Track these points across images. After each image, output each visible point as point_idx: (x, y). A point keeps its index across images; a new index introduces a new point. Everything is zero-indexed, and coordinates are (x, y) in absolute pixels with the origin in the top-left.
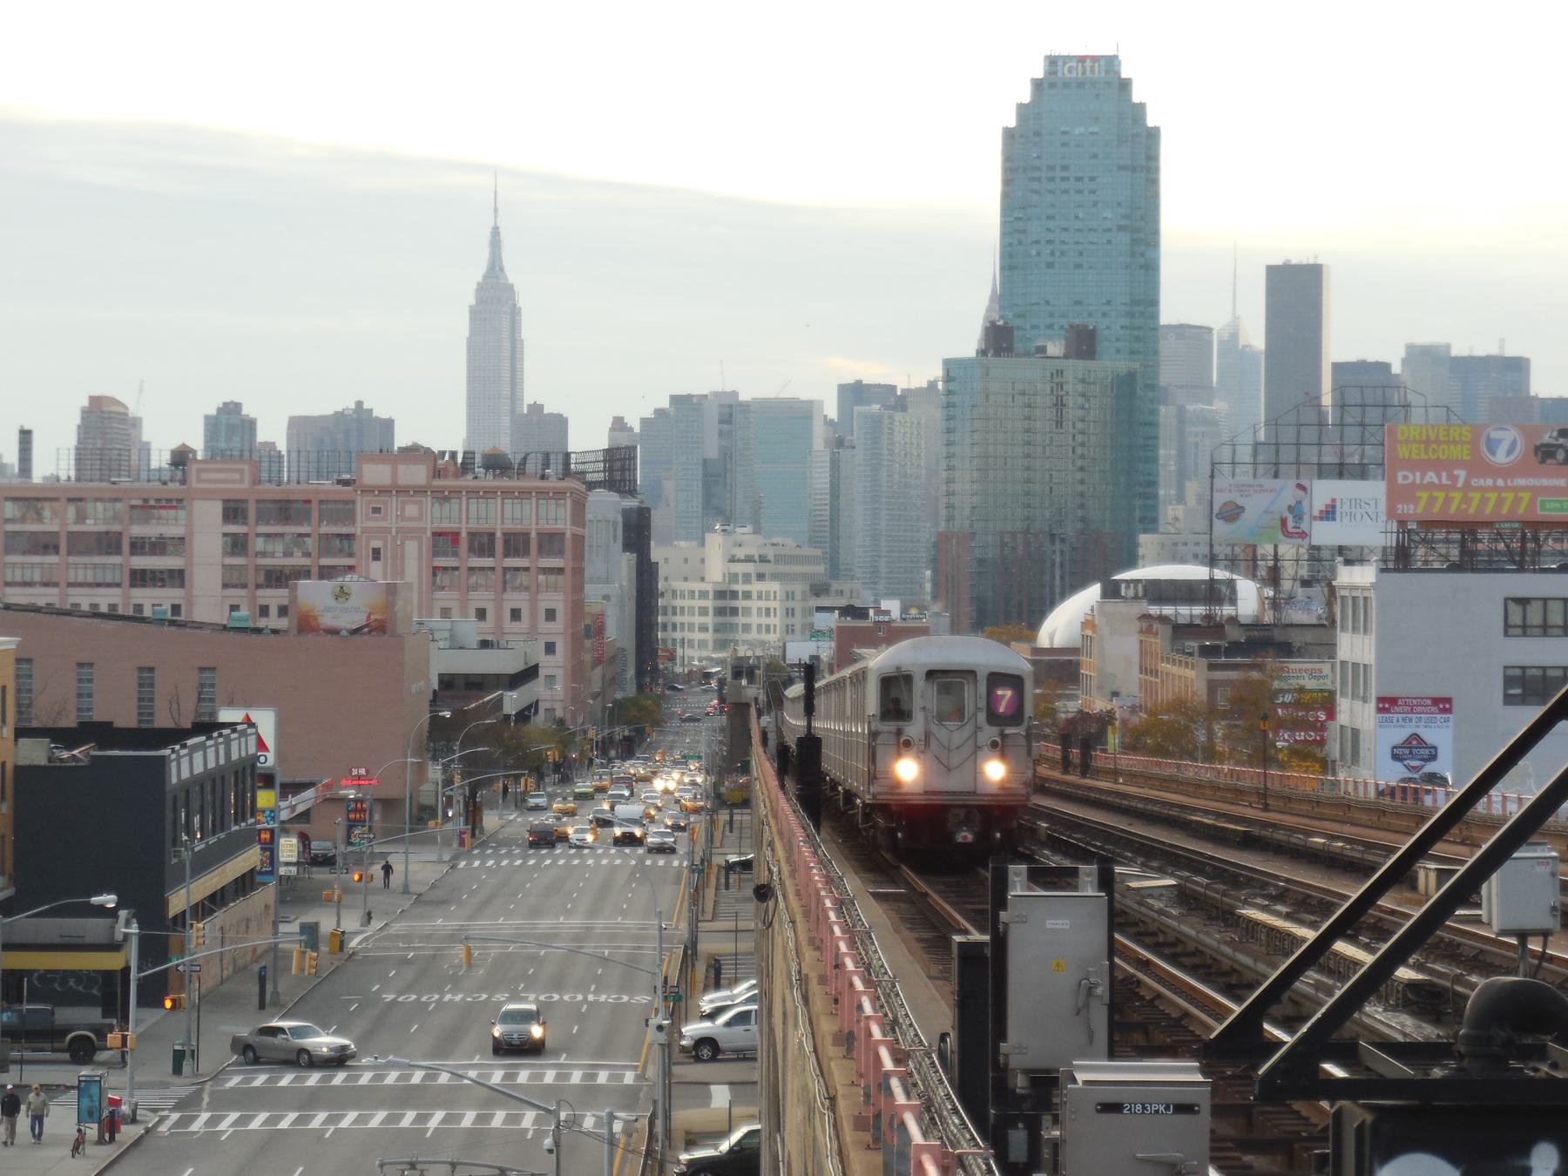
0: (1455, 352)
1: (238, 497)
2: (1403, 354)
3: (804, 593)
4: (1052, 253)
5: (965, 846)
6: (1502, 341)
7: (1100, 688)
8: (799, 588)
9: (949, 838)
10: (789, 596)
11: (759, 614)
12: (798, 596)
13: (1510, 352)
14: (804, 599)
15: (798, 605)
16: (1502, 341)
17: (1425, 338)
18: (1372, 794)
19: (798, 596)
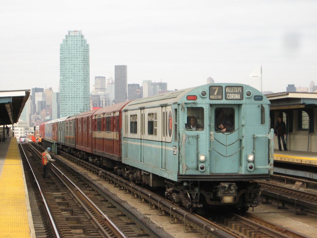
0: (152, 82)
1: (280, 211)
2: (142, 82)
3: (24, 129)
4: (70, 67)
5: (228, 205)
6: (161, 80)
7: (55, 154)
8: (23, 129)
9: (220, 199)
10: (21, 130)
11: (16, 130)
12: (23, 130)
13: (163, 82)
14: (24, 130)
15: (23, 132)
16: (161, 80)
17: (148, 79)
18: (155, 128)
19: (23, 130)
